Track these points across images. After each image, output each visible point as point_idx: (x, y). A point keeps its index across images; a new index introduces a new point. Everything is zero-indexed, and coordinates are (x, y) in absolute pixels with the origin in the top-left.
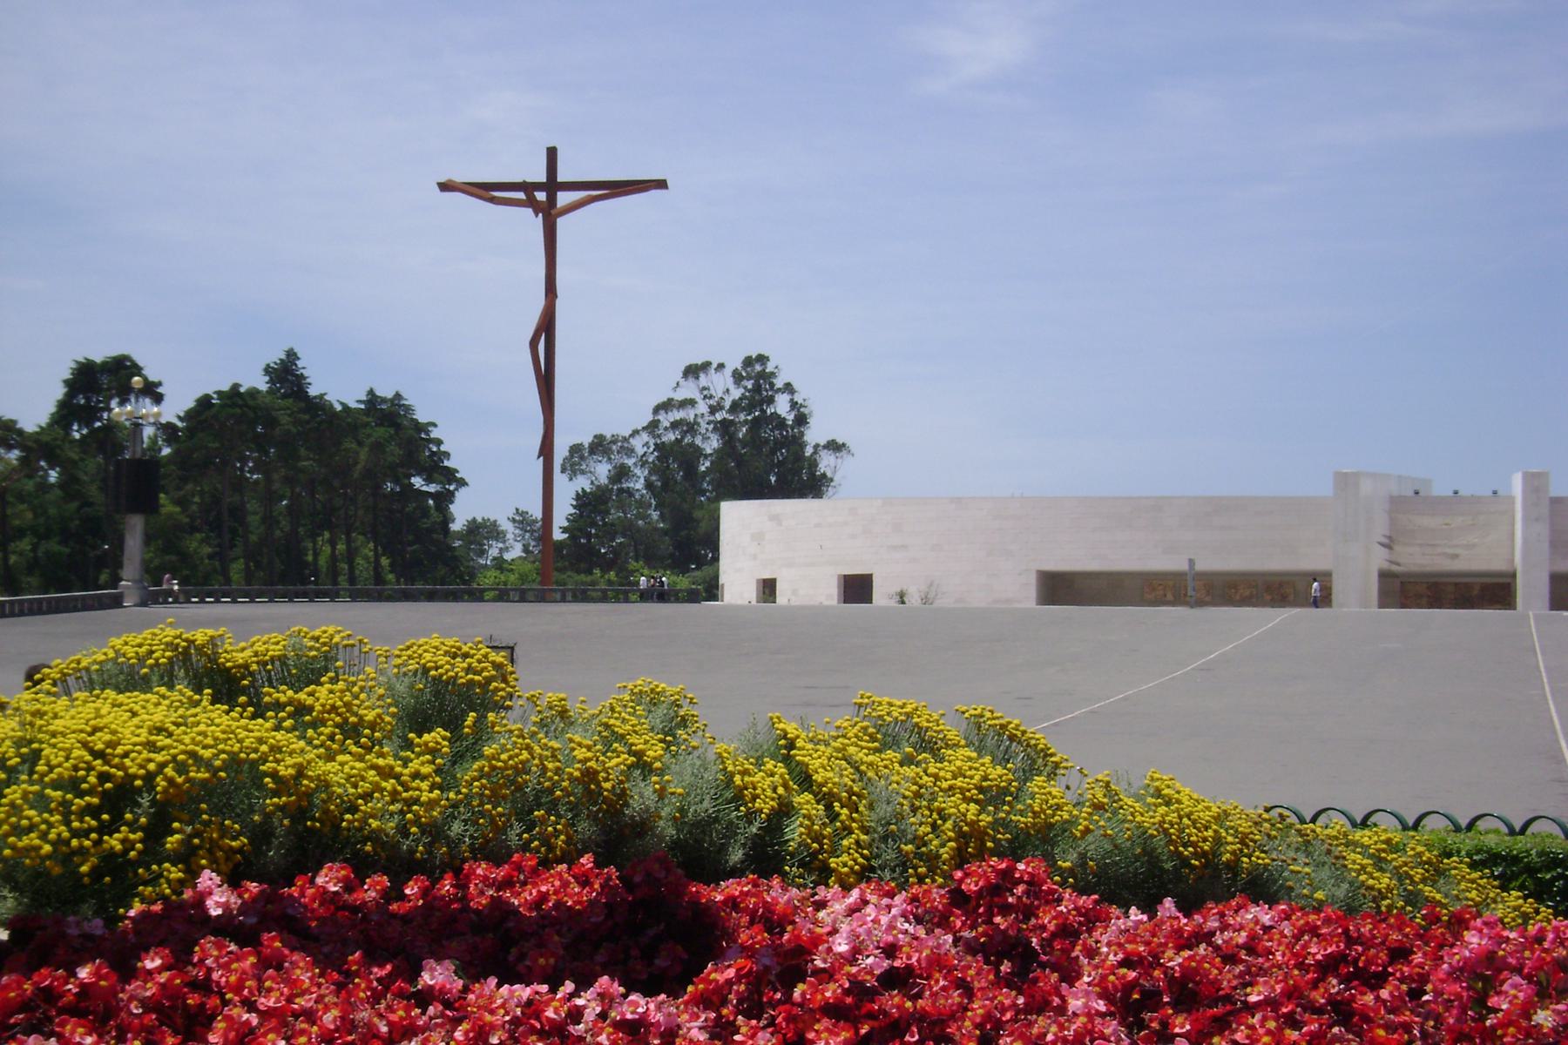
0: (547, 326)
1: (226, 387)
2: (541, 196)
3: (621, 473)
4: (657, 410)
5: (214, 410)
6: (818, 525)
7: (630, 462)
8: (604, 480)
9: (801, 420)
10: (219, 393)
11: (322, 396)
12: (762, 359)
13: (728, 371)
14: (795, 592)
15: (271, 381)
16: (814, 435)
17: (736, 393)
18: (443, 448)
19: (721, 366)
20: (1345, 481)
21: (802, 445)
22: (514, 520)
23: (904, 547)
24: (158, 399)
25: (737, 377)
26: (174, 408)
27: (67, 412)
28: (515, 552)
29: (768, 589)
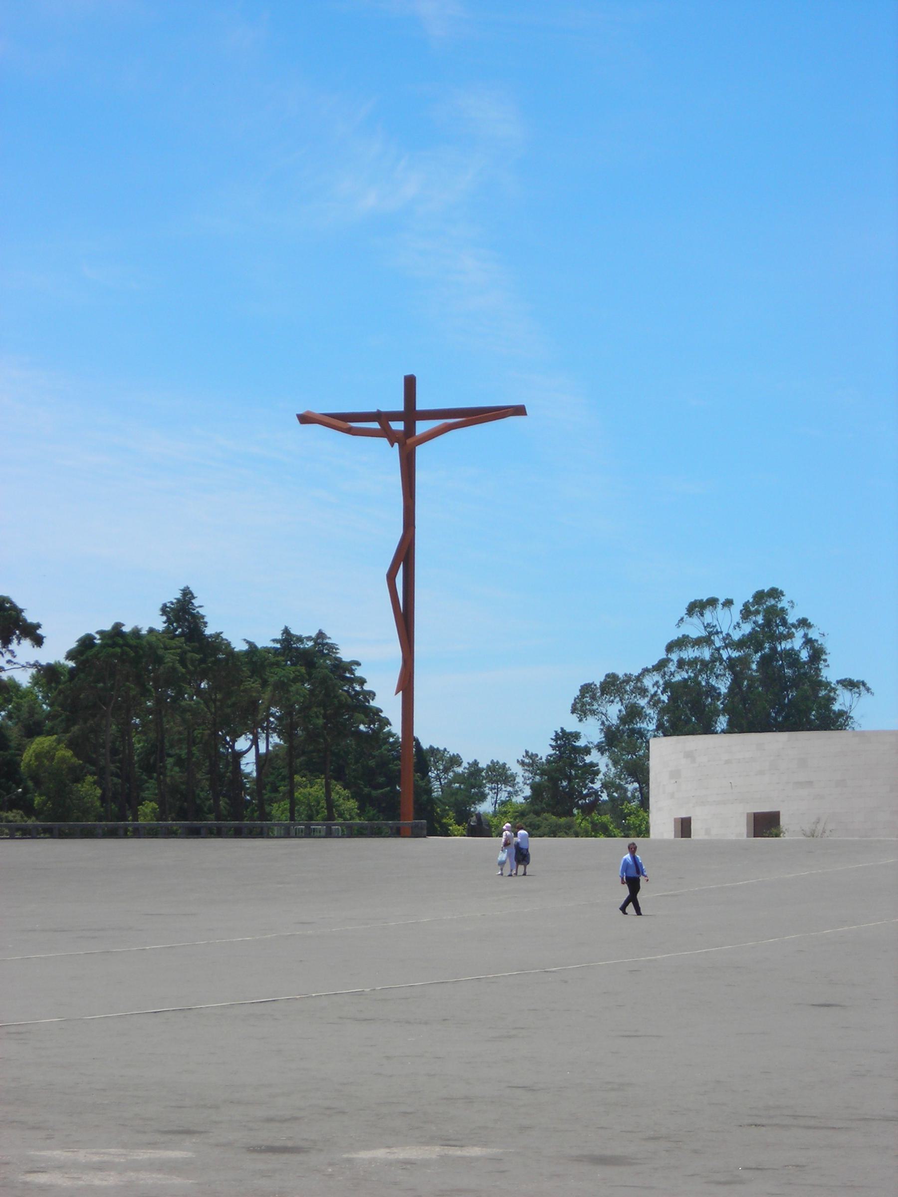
0: (405, 555)
1: (108, 627)
2: (398, 426)
3: (633, 713)
4: (670, 648)
5: (96, 649)
6: (727, 762)
7: (643, 702)
8: (615, 721)
9: (817, 654)
10: (101, 633)
11: (218, 635)
12: (775, 593)
13: (738, 607)
14: (708, 831)
15: (169, 621)
16: (831, 673)
17: (747, 628)
18: (366, 687)
19: (728, 603)
22: (523, 763)
23: (810, 783)
24: (38, 641)
26: (56, 650)
29: (684, 827)
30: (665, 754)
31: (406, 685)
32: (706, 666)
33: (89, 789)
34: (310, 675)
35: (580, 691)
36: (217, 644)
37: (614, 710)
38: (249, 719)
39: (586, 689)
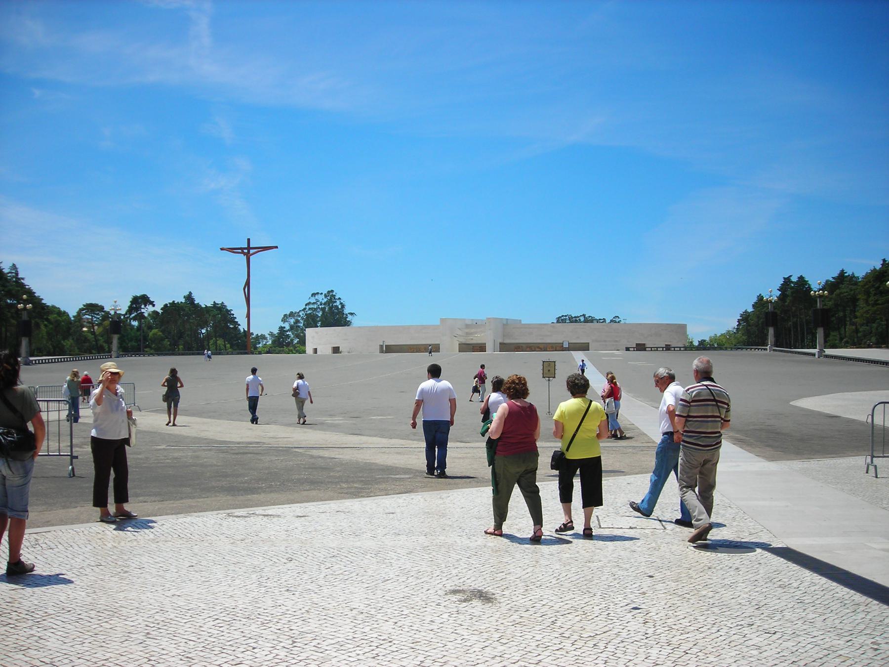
0: (248, 284)
2: (246, 251)
3: (297, 321)
9: (343, 306)
12: (332, 291)
16: (346, 311)
17: (326, 300)
20: (442, 320)
21: (108, 313)
24: (154, 306)
25: (326, 296)
26: (158, 308)
27: (131, 310)
28: (270, 342)
29: (315, 351)
30: (310, 332)
31: (248, 316)
32: (315, 309)
33: (166, 342)
34: (221, 313)
35: (65, 312)
36: (198, 305)
37: (292, 321)
38: (205, 324)
39: (285, 315)
